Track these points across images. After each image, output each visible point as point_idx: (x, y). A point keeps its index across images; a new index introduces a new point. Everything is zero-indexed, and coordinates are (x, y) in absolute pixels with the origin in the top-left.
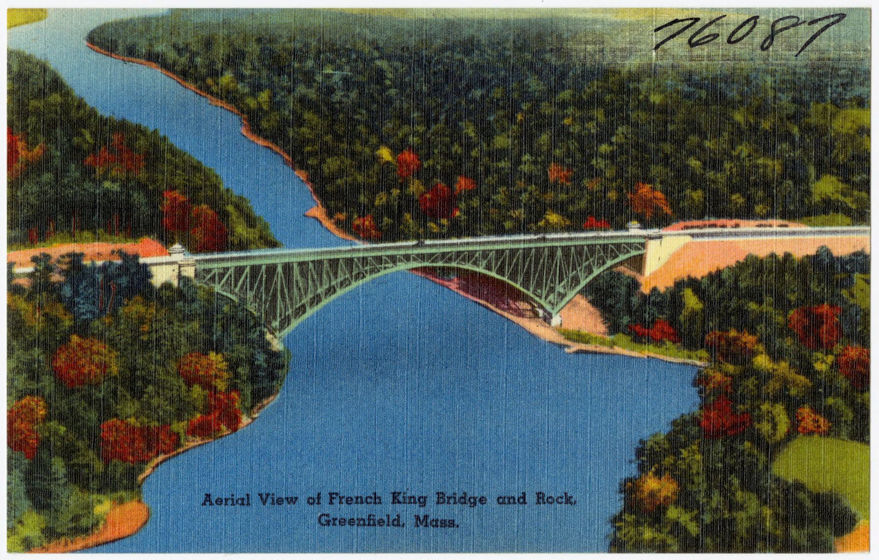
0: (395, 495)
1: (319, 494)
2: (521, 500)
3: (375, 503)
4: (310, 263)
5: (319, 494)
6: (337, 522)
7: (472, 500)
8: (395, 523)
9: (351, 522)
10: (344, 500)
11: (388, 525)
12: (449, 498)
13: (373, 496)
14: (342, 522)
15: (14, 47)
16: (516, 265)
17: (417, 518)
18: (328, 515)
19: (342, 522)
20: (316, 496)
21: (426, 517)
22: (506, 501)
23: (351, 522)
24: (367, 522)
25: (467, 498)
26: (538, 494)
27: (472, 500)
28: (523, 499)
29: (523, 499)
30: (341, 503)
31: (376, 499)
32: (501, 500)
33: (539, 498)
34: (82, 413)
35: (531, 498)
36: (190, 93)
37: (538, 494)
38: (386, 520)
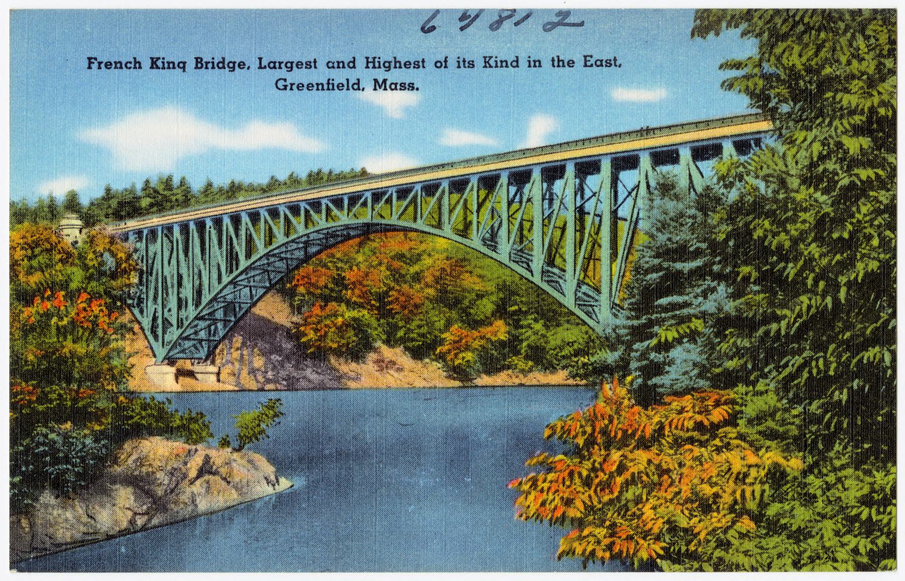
0: (199, 60)
1: (446, 58)
3: (135, 68)
4: (131, 233)
5: (446, 58)
8: (356, 87)
9: (310, 87)
10: (103, 66)
12: (207, 63)
13: (133, 60)
14: (300, 87)
15: (16, 199)
16: (237, 230)
17: (376, 81)
18: (285, 80)
19: (300, 87)
20: (443, 60)
21: (385, 81)
23: (310, 87)
24: (326, 87)
25: (226, 63)
26: (197, 59)
27: (289, 65)
28: (516, 63)
29: (137, 64)
30: (100, 68)
31: (353, 64)
33: (197, 62)
37: (197, 59)
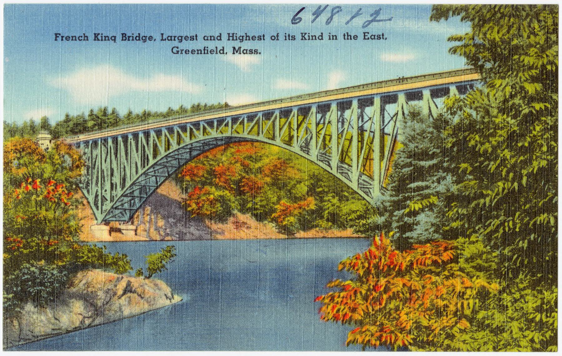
2: (138, 38)
6: (184, 52)
7: (241, 38)
9: (193, 52)
10: (64, 39)
11: (217, 53)
14: (187, 52)
17: (234, 48)
18: (177, 48)
20: (275, 35)
21: (240, 48)
22: (209, 38)
23: (193, 52)
24: (203, 52)
29: (86, 38)
32: (206, 38)
34: (209, 198)
35: (91, 37)
36: (527, 88)
38: (215, 50)
